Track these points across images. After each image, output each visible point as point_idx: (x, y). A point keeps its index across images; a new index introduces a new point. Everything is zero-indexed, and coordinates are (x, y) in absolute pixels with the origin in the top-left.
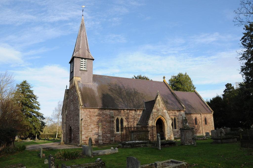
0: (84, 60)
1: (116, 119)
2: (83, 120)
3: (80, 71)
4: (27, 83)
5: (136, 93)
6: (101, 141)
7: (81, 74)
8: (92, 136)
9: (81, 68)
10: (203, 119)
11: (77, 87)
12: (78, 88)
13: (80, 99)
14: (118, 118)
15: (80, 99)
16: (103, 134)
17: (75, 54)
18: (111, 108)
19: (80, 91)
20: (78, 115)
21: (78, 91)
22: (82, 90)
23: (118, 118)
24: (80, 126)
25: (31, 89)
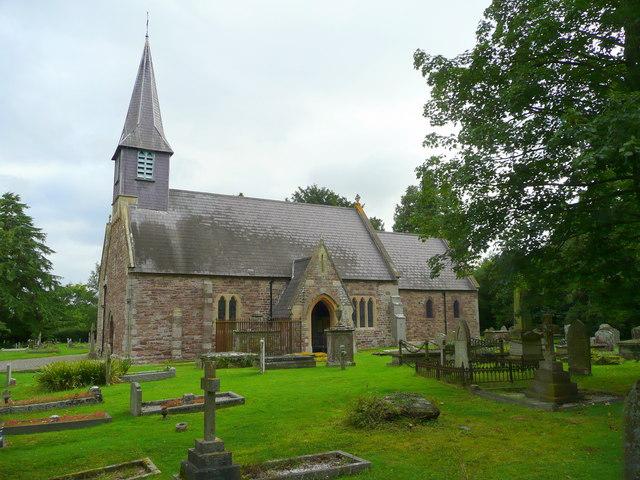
0: (146, 156)
5: (279, 239)
6: (179, 352)
7: (139, 189)
9: (140, 176)
10: (450, 304)
11: (127, 221)
12: (127, 224)
14: (222, 298)
17: (356, 461)
23: (222, 298)
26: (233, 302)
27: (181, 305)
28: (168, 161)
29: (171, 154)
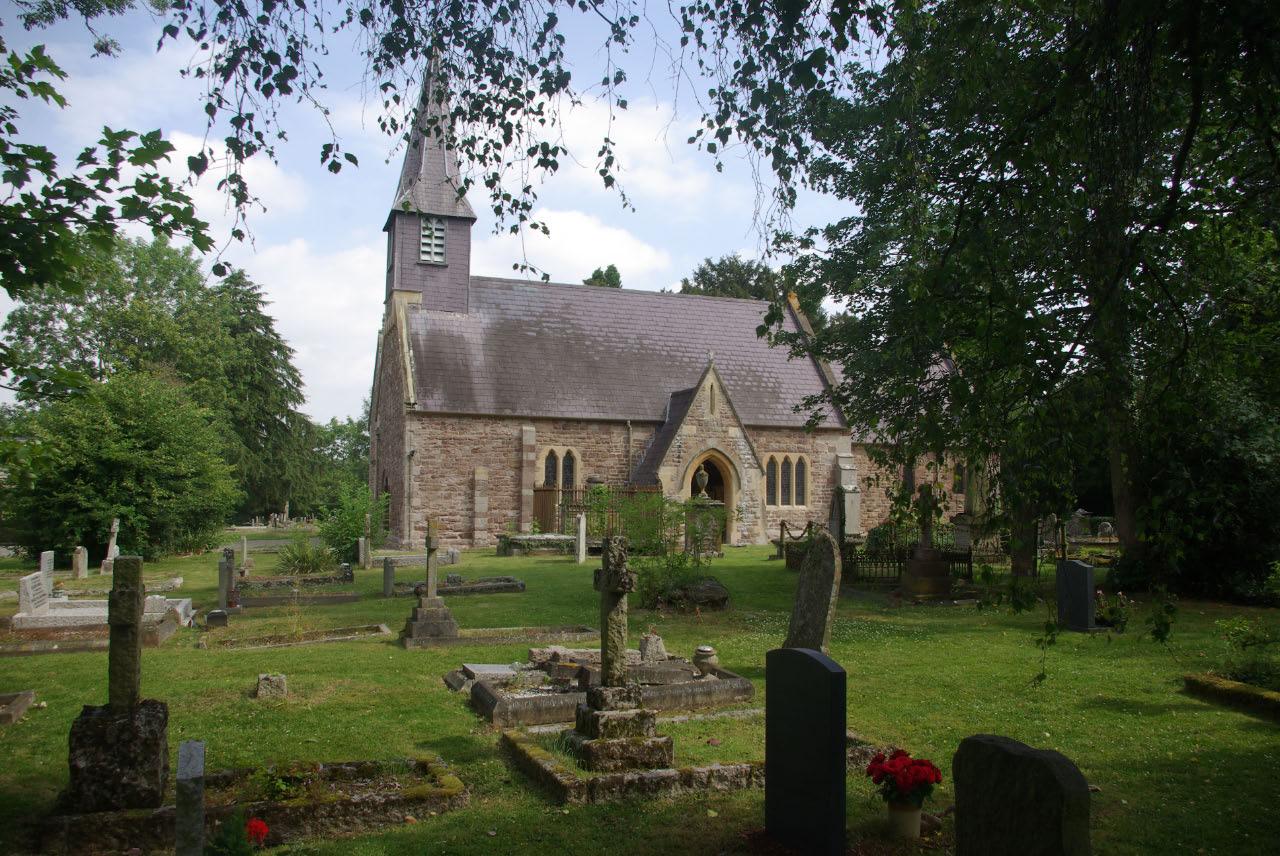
1: (545, 453)
2: (417, 456)
3: (418, 268)
4: (248, 279)
8: (450, 514)
9: (424, 257)
11: (404, 331)
13: (410, 381)
14: (552, 453)
15: (410, 381)
16: (490, 509)
18: (526, 412)
19: (414, 344)
20: (401, 437)
21: (406, 348)
22: (421, 343)
23: (552, 453)
24: (406, 476)
25: (265, 311)
26: (569, 458)
27: (487, 464)
28: (469, 231)
29: (473, 220)
